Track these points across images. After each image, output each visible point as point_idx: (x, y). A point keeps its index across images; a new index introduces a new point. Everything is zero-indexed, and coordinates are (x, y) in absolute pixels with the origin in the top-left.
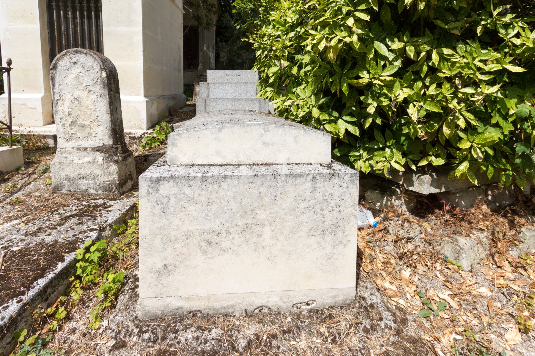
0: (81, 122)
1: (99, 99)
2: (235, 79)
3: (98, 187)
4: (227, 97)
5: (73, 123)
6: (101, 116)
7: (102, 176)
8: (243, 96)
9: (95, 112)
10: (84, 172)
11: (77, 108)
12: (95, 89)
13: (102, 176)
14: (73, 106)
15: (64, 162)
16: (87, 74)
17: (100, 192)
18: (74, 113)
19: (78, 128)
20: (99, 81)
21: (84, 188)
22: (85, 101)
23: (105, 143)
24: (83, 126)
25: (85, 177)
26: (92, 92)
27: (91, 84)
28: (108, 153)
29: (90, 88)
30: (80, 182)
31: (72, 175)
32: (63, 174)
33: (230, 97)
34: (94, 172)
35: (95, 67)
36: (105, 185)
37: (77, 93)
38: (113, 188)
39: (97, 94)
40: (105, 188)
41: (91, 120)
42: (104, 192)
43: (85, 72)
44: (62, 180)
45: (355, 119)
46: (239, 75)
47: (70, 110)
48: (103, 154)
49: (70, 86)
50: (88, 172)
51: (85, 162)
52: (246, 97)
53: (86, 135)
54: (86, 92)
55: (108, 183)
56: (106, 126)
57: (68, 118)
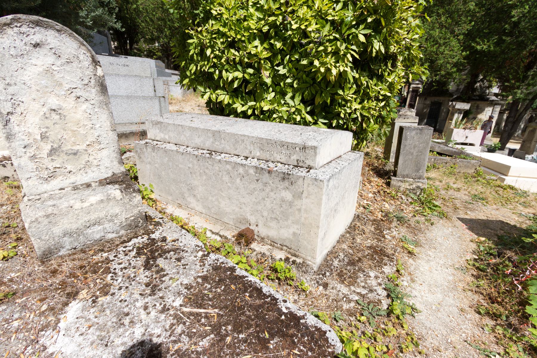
0: (69, 147)
1: (96, 110)
2: (123, 70)
3: (119, 228)
4: (120, 94)
5: (53, 152)
6: (105, 135)
7: (124, 213)
8: (139, 94)
9: (92, 131)
10: (93, 217)
11: (57, 126)
12: (87, 94)
13: (124, 213)
14: (48, 123)
15: (55, 212)
16: (68, 68)
17: (123, 232)
18: (52, 134)
19: (66, 157)
20: (93, 81)
21: (97, 236)
22: (73, 114)
23: (115, 172)
24: (75, 154)
25: (98, 222)
26: (82, 99)
27: (80, 86)
28: (124, 183)
29: (79, 93)
30: (89, 231)
31: (74, 227)
32: (57, 230)
33: (125, 94)
34: (112, 211)
35: (81, 57)
36: (129, 222)
37: (53, 102)
38: (140, 222)
39: (92, 102)
40: (130, 225)
41: (88, 143)
42: (129, 231)
43: (62, 65)
44: (56, 239)
45: (327, 121)
46: (127, 66)
47: (44, 130)
48: (117, 186)
49: (34, 88)
50: (102, 214)
51: (94, 202)
52: (143, 94)
53: (82, 166)
54: (71, 99)
55: (132, 218)
56: (113, 148)
57: (42, 144)
